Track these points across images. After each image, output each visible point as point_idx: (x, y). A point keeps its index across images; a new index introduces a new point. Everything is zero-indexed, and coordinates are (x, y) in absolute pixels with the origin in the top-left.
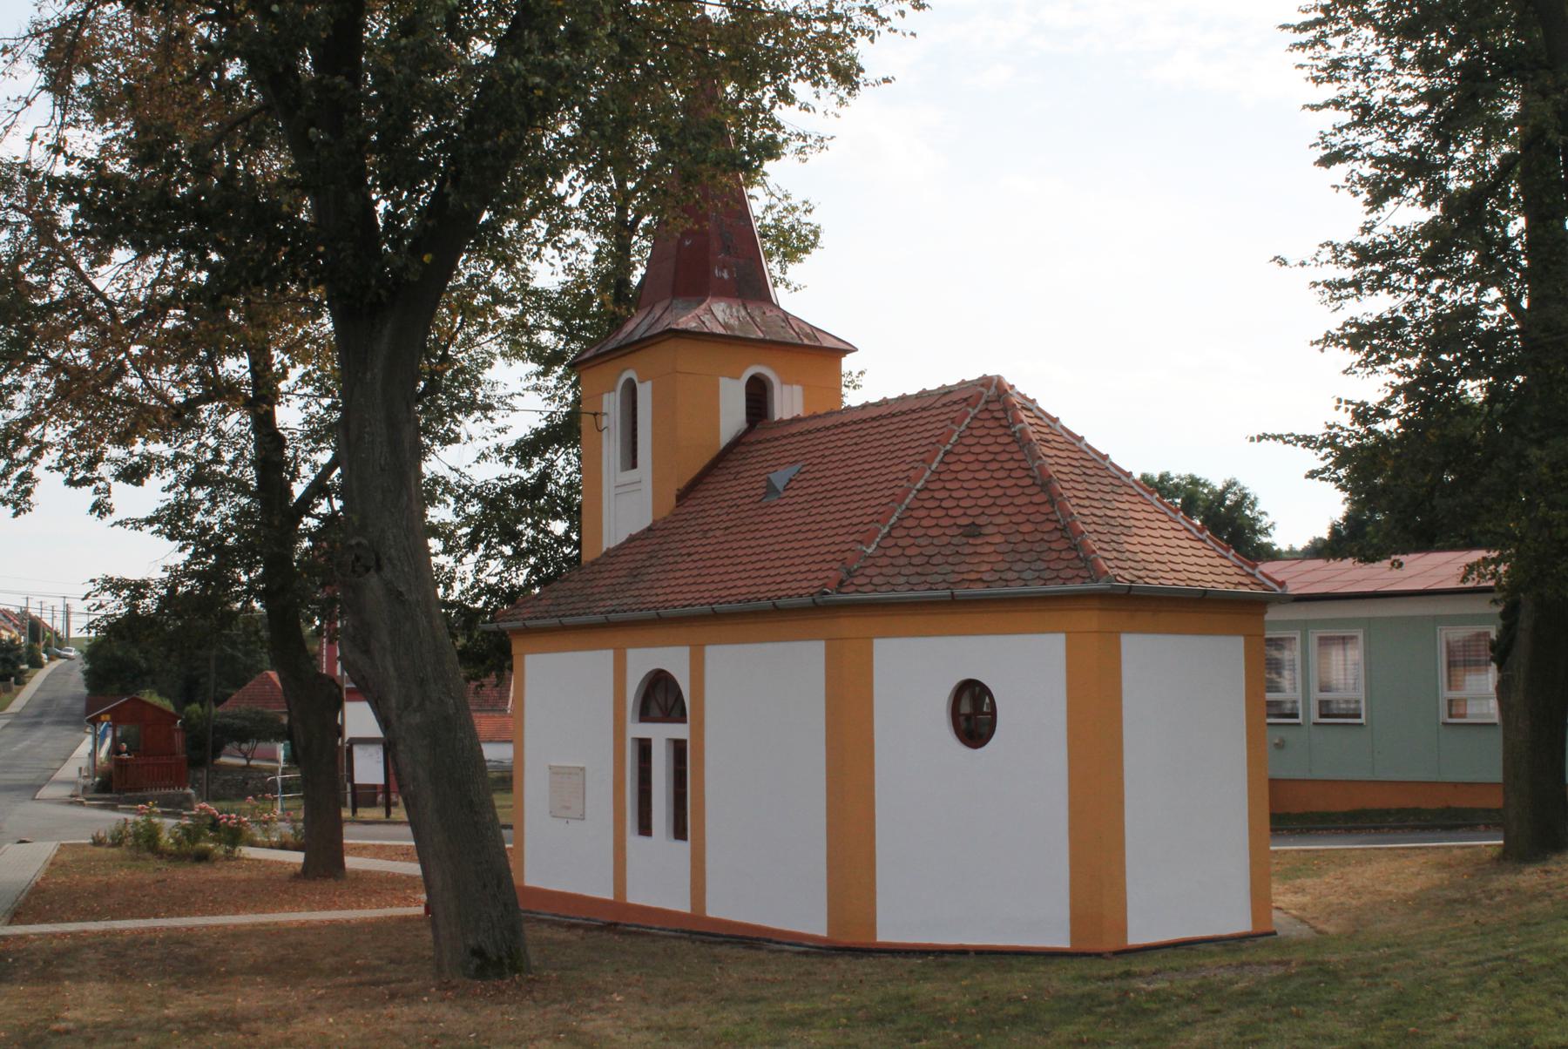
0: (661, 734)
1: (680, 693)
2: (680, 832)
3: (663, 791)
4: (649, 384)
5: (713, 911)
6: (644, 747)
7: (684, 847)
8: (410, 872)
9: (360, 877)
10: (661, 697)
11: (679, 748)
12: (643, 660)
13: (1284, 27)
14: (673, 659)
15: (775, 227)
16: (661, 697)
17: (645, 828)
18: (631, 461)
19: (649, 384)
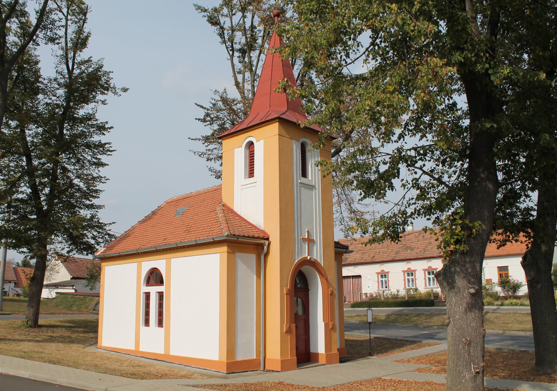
0: (154, 290)
1: (161, 275)
2: (160, 323)
3: (155, 311)
4: (262, 142)
6: (148, 295)
7: (162, 330)
8: (443, 349)
9: (258, 354)
10: (155, 277)
11: (161, 295)
13: (196, 104)
14: (158, 263)
16: (155, 277)
17: (147, 323)
18: (251, 173)
19: (262, 142)
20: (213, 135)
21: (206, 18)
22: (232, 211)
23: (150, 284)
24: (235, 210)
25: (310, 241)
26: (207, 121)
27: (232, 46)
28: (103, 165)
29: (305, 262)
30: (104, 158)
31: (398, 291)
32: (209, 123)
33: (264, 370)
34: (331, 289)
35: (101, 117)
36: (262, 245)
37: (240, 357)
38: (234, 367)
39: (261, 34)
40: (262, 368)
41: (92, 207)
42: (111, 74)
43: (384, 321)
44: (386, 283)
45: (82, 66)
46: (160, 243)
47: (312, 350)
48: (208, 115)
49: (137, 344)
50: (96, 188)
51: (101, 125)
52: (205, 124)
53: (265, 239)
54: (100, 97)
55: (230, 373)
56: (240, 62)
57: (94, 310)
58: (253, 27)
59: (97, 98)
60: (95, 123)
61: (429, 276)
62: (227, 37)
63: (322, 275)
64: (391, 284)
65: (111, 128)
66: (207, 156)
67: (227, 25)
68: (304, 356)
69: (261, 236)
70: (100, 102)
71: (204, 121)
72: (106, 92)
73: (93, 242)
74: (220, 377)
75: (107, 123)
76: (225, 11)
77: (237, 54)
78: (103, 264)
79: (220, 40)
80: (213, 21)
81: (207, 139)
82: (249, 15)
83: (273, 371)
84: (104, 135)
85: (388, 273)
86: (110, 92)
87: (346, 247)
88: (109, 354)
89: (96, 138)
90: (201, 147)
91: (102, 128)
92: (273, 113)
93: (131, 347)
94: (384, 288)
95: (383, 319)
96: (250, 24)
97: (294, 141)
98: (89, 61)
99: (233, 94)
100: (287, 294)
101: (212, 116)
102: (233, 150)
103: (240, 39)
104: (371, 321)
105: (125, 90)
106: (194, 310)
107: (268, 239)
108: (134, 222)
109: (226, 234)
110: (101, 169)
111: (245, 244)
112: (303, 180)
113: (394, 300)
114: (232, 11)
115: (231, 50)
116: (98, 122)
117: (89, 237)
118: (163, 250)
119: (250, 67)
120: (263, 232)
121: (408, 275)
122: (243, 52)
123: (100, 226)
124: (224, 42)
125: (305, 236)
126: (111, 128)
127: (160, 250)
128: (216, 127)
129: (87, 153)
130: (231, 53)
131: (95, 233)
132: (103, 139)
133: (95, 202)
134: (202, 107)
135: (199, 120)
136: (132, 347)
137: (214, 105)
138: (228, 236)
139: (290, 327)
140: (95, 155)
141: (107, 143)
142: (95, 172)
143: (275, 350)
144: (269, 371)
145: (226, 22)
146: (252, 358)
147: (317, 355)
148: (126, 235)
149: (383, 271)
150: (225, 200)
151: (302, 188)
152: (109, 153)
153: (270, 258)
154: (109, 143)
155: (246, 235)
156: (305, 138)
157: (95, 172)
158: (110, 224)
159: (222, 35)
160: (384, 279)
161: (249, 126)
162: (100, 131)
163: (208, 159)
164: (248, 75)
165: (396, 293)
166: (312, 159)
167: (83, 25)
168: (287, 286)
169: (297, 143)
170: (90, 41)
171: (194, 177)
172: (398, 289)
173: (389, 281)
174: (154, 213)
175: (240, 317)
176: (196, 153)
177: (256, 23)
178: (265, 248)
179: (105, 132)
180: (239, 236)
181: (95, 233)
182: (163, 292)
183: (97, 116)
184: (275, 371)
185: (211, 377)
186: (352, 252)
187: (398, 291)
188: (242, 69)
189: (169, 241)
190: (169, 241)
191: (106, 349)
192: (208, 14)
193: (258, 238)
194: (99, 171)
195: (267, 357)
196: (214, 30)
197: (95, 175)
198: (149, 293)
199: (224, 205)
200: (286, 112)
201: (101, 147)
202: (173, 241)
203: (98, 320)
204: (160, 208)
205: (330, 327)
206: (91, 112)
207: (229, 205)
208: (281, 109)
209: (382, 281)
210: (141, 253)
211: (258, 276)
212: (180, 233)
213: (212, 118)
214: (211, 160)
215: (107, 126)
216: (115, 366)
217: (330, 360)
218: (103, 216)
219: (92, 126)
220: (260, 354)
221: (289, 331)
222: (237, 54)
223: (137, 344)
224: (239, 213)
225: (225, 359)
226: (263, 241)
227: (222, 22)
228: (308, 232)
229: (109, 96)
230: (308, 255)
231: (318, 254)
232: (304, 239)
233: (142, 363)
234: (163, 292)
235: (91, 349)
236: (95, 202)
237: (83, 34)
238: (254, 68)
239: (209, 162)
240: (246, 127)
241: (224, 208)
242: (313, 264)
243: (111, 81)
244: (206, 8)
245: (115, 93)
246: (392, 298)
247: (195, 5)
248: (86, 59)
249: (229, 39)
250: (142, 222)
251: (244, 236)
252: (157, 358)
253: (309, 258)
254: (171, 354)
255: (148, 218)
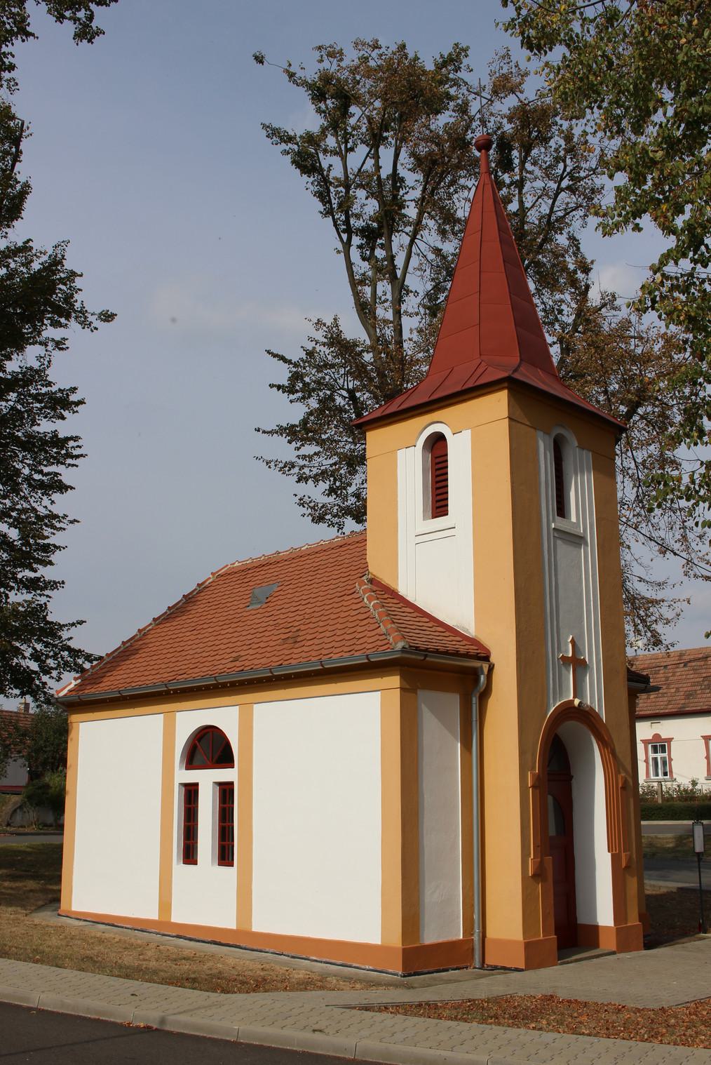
0: (207, 779)
2: (225, 856)
3: (211, 826)
4: (467, 434)
5: (177, 917)
6: (191, 792)
7: (230, 873)
9: (468, 929)
10: (210, 748)
11: (226, 791)
12: (190, 719)
13: (269, 352)
14: (222, 716)
15: (36, 453)
16: (210, 748)
17: (190, 855)
18: (438, 504)
19: (467, 434)
20: (305, 422)
21: (288, 158)
22: (394, 594)
23: (196, 763)
24: (402, 591)
25: (578, 664)
26: (297, 391)
27: (347, 222)
28: (63, 488)
29: (568, 712)
30: (66, 475)
31: (694, 783)
32: (300, 394)
33: (482, 968)
34: (623, 774)
35: (60, 376)
36: (475, 673)
37: (430, 937)
38: (421, 959)
39: (417, 194)
40: (477, 963)
41: (33, 585)
42: (77, 279)
43: (672, 850)
44: (664, 763)
45: (10, 261)
46: (224, 667)
47: (582, 919)
48: (296, 377)
49: (165, 905)
50: (46, 541)
51: (59, 395)
52: (292, 397)
53: (478, 657)
54: (50, 332)
55: (410, 975)
56: (364, 259)
57: (8, 825)
58: (395, 176)
59: (45, 334)
60: (44, 390)
61: (655, 755)
62: (335, 202)
63: (605, 743)
64: (676, 767)
65: (81, 402)
66: (296, 470)
67: (337, 172)
68: (568, 934)
69: (473, 652)
70: (50, 344)
71: (290, 390)
72: (63, 320)
73: (34, 666)
74: (389, 984)
75: (74, 390)
76: (331, 141)
77: (356, 240)
78: (74, 718)
79: (321, 208)
80: (306, 162)
81: (292, 433)
82: (386, 154)
83: (504, 968)
84: (63, 418)
85: (669, 740)
86: (73, 320)
87: (645, 679)
88: (111, 933)
89: (45, 426)
90: (285, 450)
91: (61, 403)
92: (490, 369)
93: (150, 912)
94: (661, 776)
95: (671, 845)
96: (390, 171)
97: (540, 434)
98: (26, 248)
99: (354, 330)
100: (533, 786)
101: (307, 379)
102: (394, 452)
103: (367, 207)
104: (702, 850)
105: (107, 317)
106: (317, 825)
107: (486, 658)
108: (144, 621)
109: (400, 645)
110: (56, 496)
111: (437, 671)
112: (558, 523)
113: (685, 803)
114: (346, 142)
115: (344, 231)
116: (54, 389)
117: (27, 654)
118: (233, 684)
119: (387, 270)
120: (474, 641)
121: (655, 751)
122: (370, 235)
123: (51, 631)
124: (329, 212)
125: (567, 651)
126: (81, 402)
127: (224, 685)
128: (314, 403)
129: (22, 462)
130: (345, 236)
131: (39, 647)
132: (64, 427)
133: (45, 572)
134: (282, 358)
135: (279, 387)
136: (152, 913)
137: (310, 354)
138: (404, 650)
139: (541, 862)
140: (40, 464)
141: (72, 438)
142: (43, 504)
143: (507, 919)
144: (495, 968)
145: (333, 166)
146: (454, 938)
147: (595, 929)
148: (127, 651)
149: (657, 736)
150: (376, 567)
151: (559, 542)
152: (69, 461)
153: (492, 703)
154: (76, 439)
155: (442, 649)
156: (564, 427)
157: (43, 504)
158: (73, 624)
159: (323, 196)
160: (659, 755)
161: (433, 397)
162: (54, 409)
163: (302, 479)
164: (384, 287)
165: (691, 787)
166: (582, 473)
167: (13, 166)
168: (533, 768)
169: (547, 437)
170: (29, 204)
171: (272, 518)
172: (695, 777)
173: (671, 760)
174: (189, 599)
175: (431, 841)
176: (272, 464)
177: (402, 172)
178: (482, 678)
179: (66, 413)
180: (427, 650)
181: (39, 647)
182: (232, 784)
183: (51, 375)
184: (510, 969)
185: (371, 984)
186: (656, 689)
187: (694, 783)
188: (370, 273)
189: (247, 663)
190: (247, 663)
191: (81, 917)
192: (296, 147)
193: (467, 656)
194: (53, 502)
195: (490, 934)
196: (303, 184)
197: (42, 511)
198: (196, 785)
199: (371, 581)
200: (519, 366)
201: (59, 449)
202: (259, 663)
203: (59, 850)
204: (202, 588)
205: (624, 865)
206: (36, 365)
207: (386, 580)
208: (510, 362)
209: (655, 760)
210: (175, 691)
211: (467, 745)
212: (272, 644)
213: (305, 384)
214: (306, 480)
215: (73, 398)
216: (129, 959)
217: (624, 945)
218: (58, 609)
219: (37, 398)
220: (473, 929)
221: (539, 875)
222: (356, 240)
223: (165, 905)
224: (410, 598)
225: (396, 941)
226: (477, 664)
227: (325, 165)
228: (573, 642)
229: (72, 331)
230: (575, 697)
231: (594, 695)
232: (564, 658)
233: (186, 953)
234: (232, 784)
235: (44, 918)
236: (45, 572)
237: (13, 187)
238: (399, 273)
239: (302, 484)
240: (426, 399)
241: (375, 588)
242: (583, 715)
243: (76, 296)
244: (291, 133)
245: (85, 323)
246: (680, 798)
247: (265, 126)
248: (20, 244)
249: (340, 205)
250: (160, 621)
251: (437, 651)
252: (216, 938)
253: (577, 702)
254: (256, 928)
255: (175, 612)
